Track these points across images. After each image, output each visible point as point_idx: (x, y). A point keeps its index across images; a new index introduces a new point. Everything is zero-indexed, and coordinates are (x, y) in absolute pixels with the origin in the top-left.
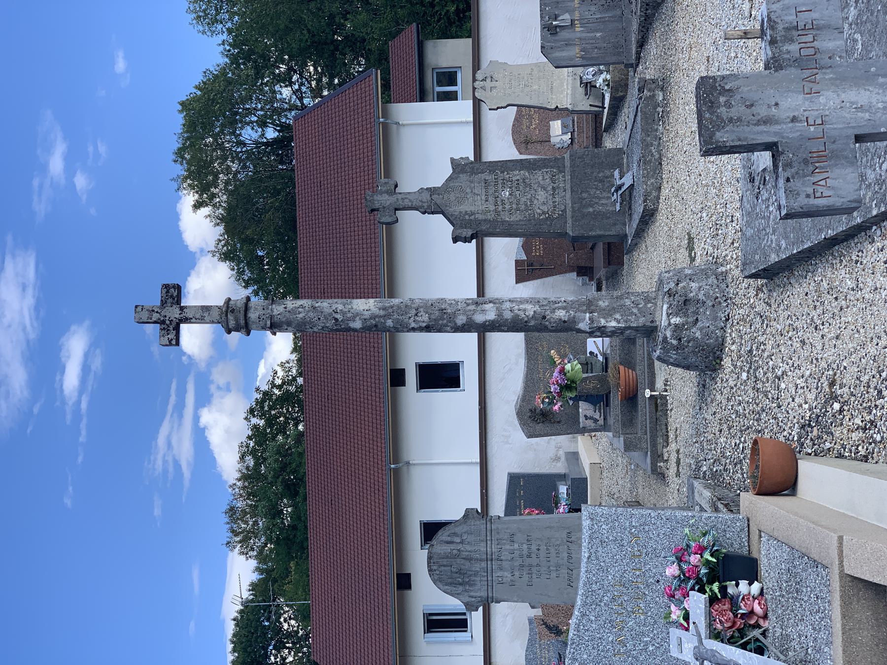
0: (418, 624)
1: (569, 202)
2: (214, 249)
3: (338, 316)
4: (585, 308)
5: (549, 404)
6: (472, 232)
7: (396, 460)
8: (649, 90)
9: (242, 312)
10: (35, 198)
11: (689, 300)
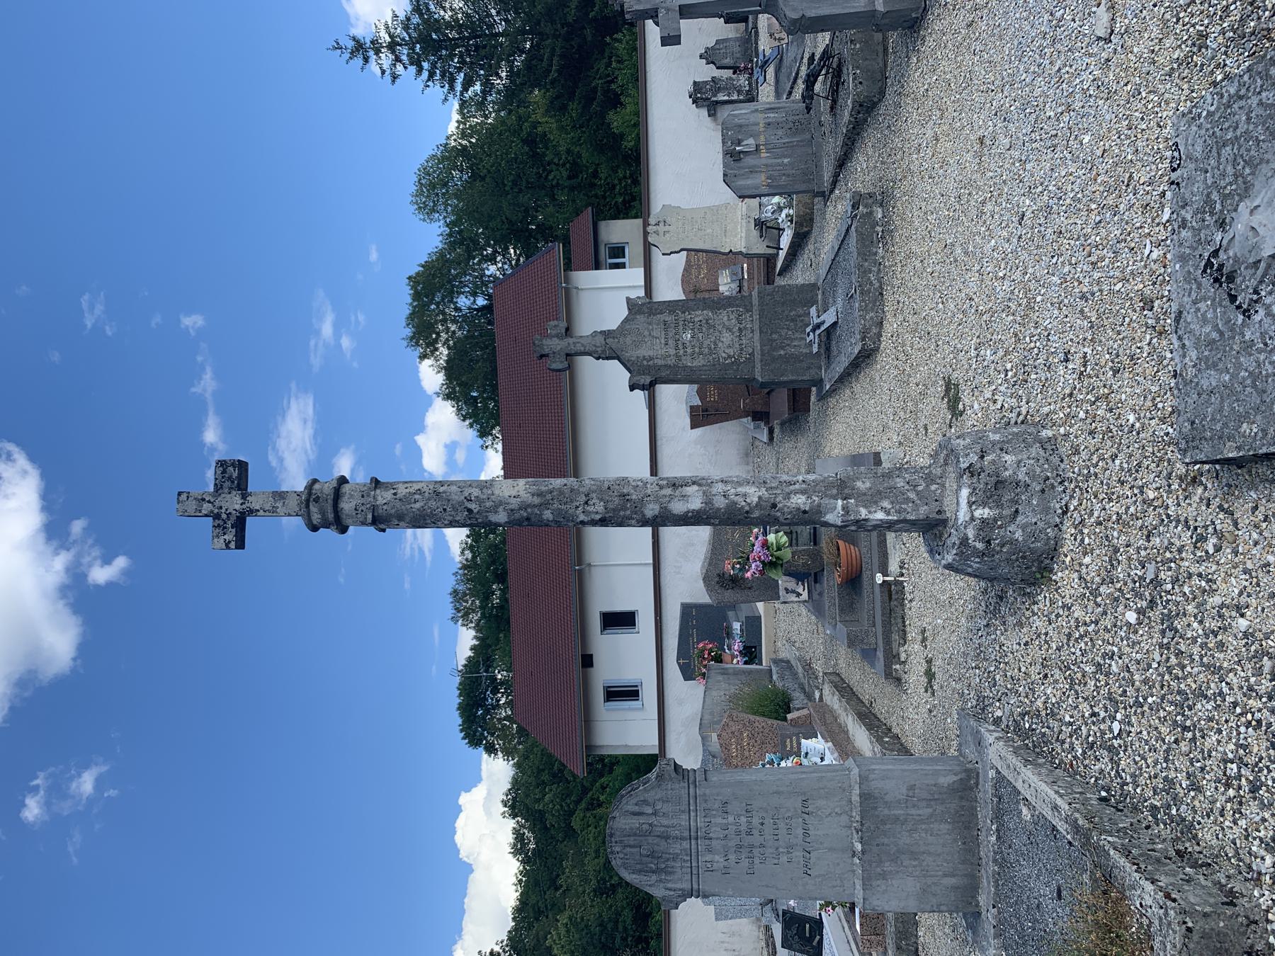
0: (599, 695)
1: (757, 345)
3: (473, 506)
4: (835, 491)
5: (740, 570)
6: (647, 380)
8: (866, 206)
9: (330, 502)
11: (1001, 482)
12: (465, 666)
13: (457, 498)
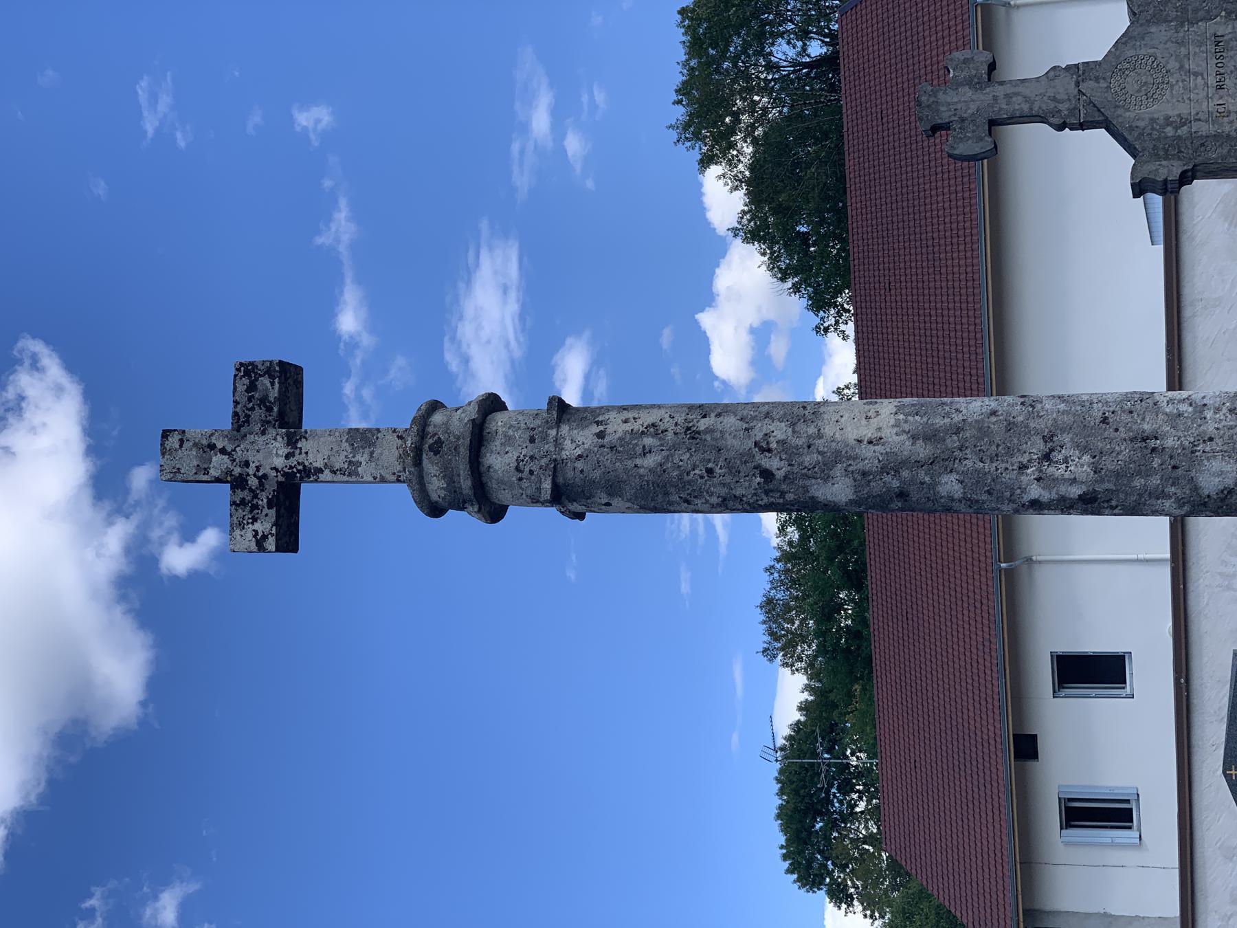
0: (1051, 815)
2: (737, 225)
3: (773, 463)
7: (1010, 557)
9: (464, 451)
10: (516, 168)
12: (789, 738)
13: (737, 444)
